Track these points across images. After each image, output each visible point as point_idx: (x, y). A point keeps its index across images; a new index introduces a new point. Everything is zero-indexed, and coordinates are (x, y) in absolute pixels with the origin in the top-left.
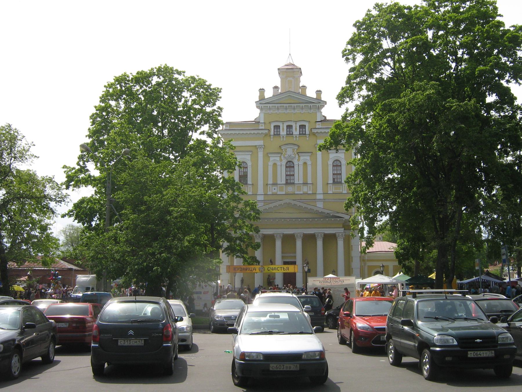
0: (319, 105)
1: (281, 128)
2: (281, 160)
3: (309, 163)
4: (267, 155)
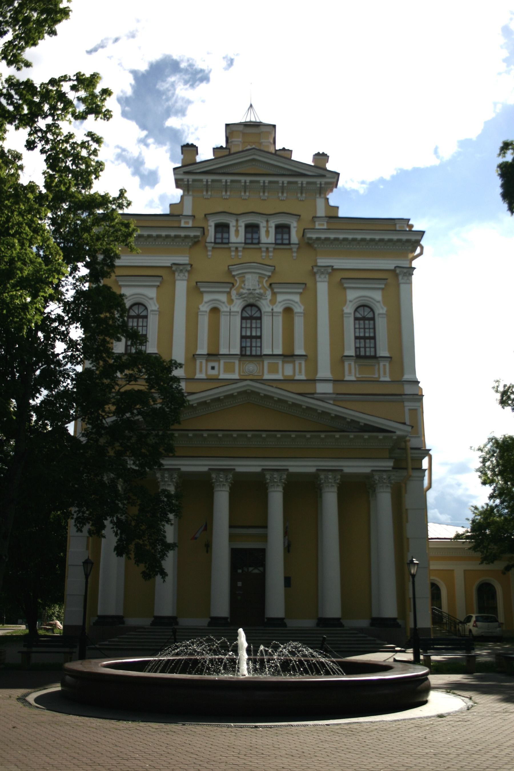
0: (323, 180)
1: (232, 230)
2: (231, 301)
3: (298, 309)
4: (196, 290)
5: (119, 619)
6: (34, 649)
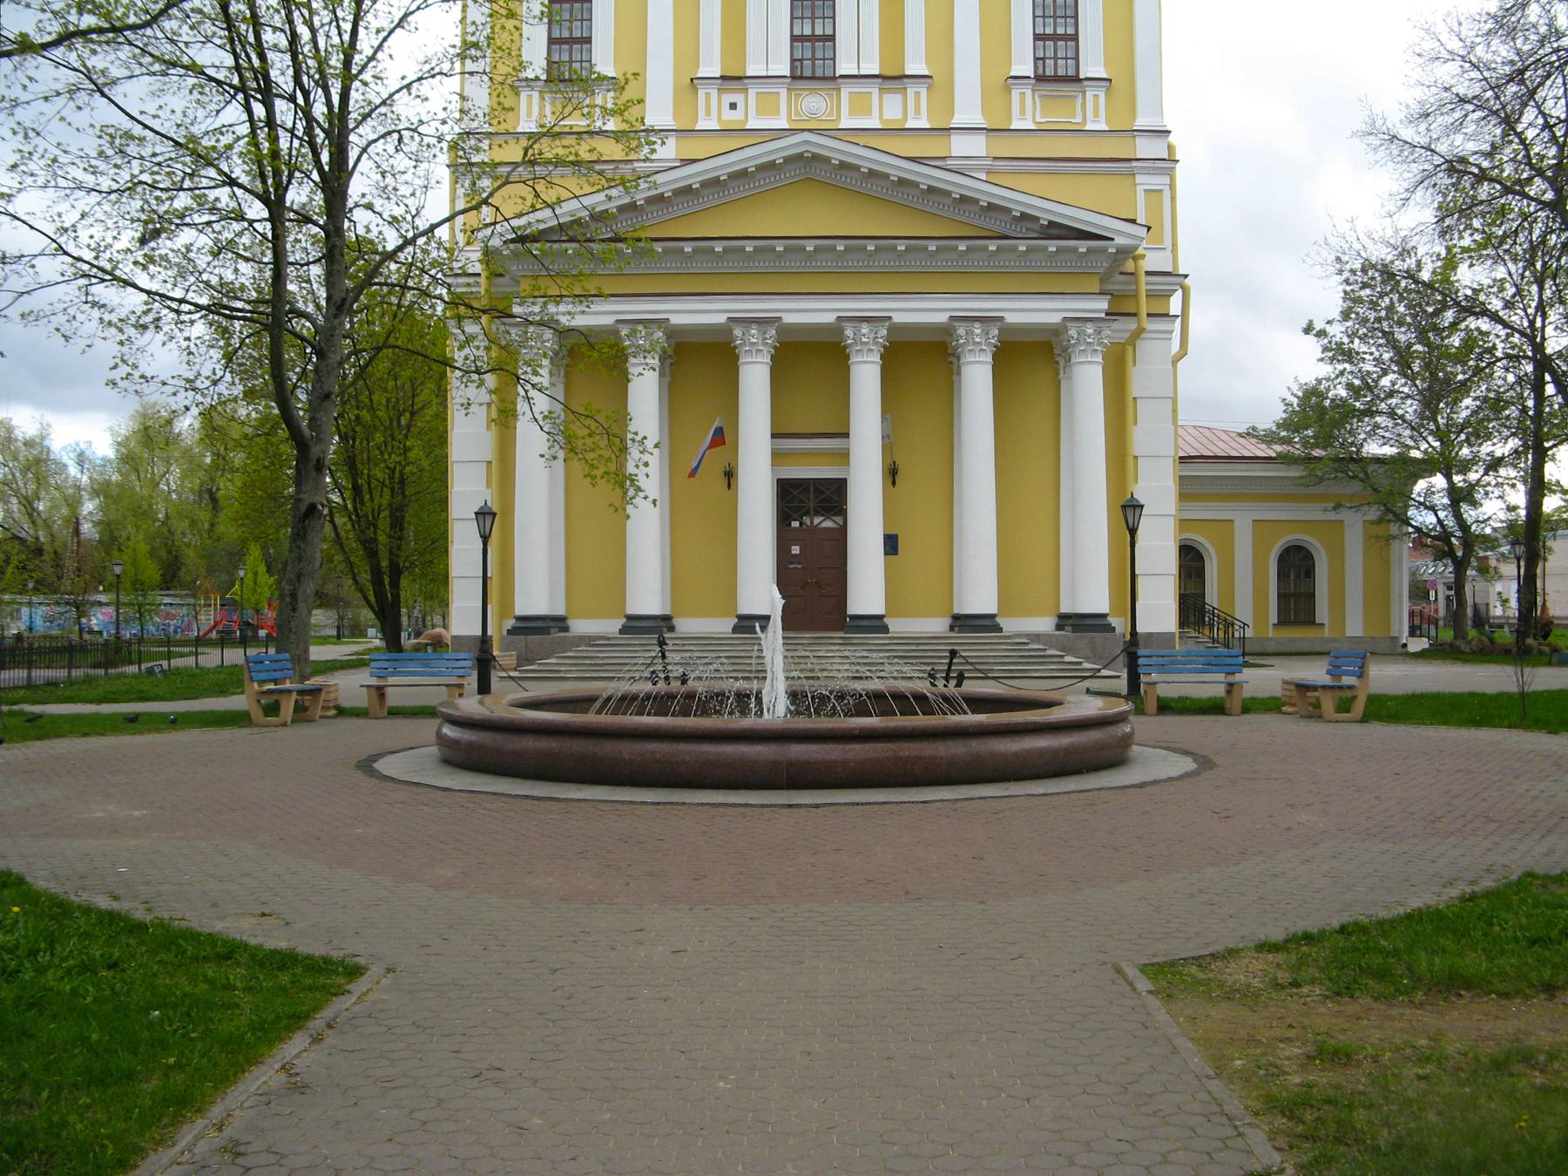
5: (560, 622)
6: (391, 680)
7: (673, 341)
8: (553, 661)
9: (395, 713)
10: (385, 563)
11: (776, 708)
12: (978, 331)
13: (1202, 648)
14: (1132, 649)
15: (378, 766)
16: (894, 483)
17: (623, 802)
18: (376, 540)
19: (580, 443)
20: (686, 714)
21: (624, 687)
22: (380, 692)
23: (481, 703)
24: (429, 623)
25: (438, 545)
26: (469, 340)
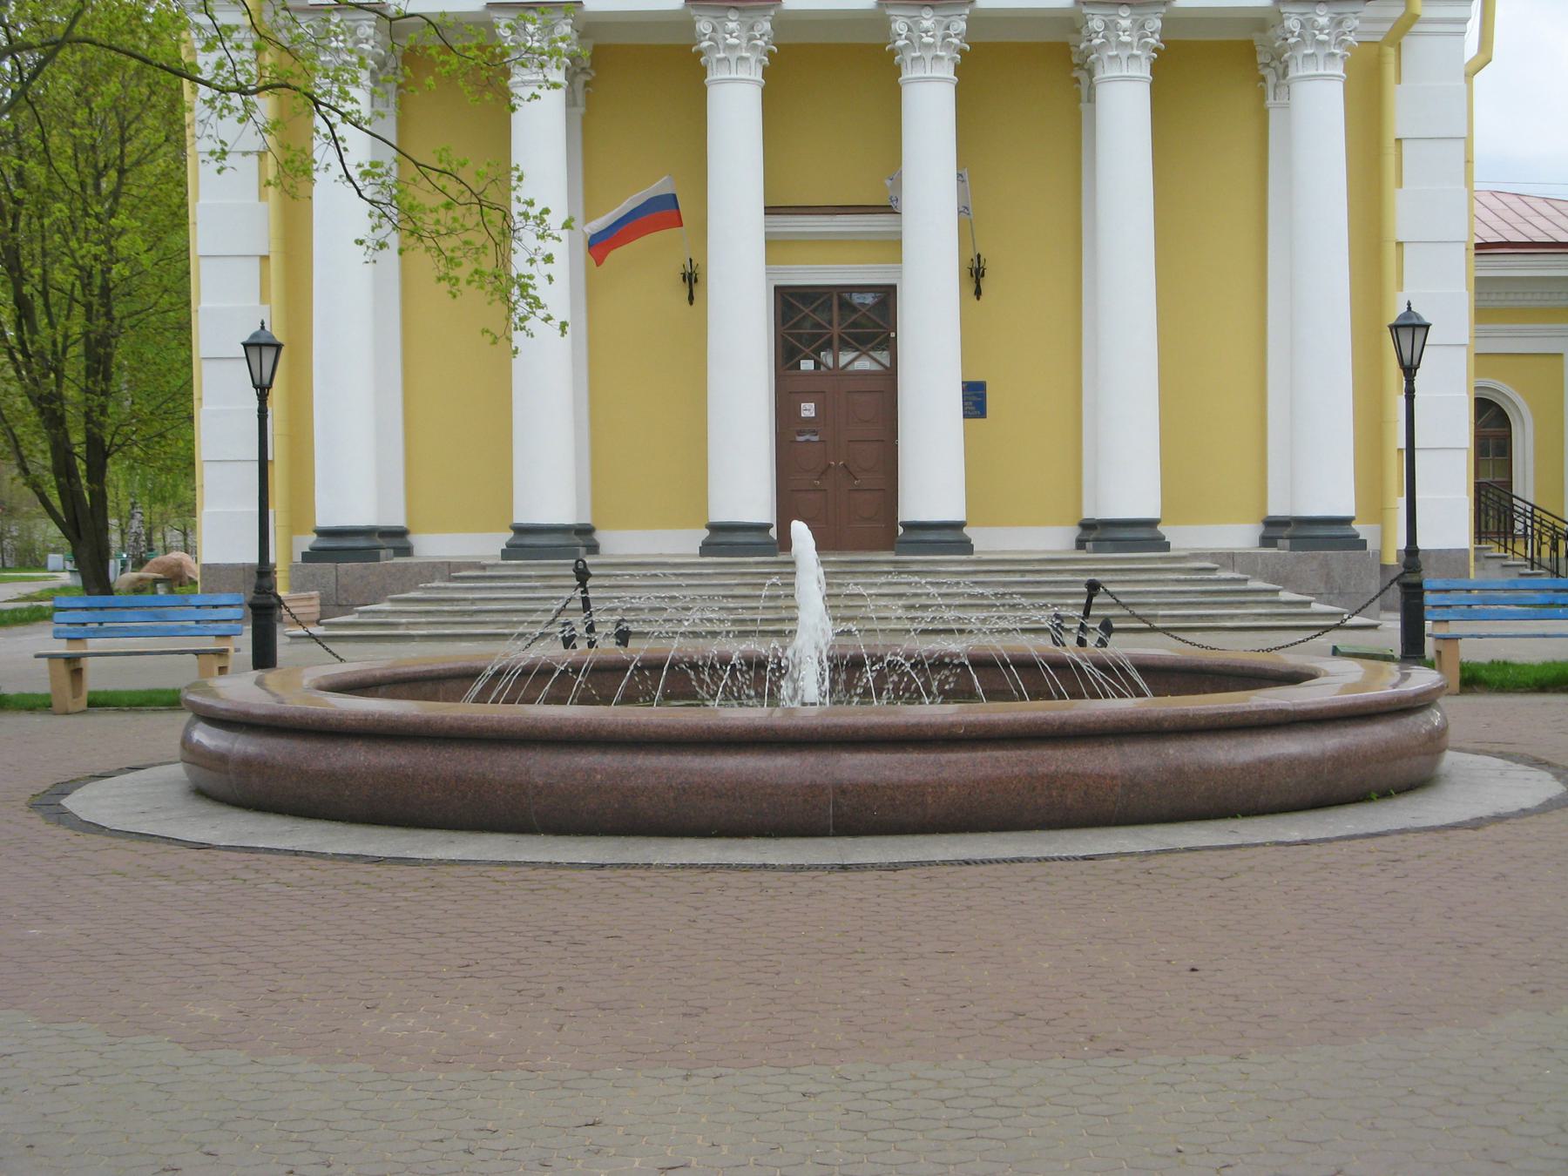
5: (397, 539)
6: (94, 644)
7: (590, 42)
8: (386, 606)
9: (99, 703)
10: (77, 438)
11: (807, 691)
12: (1125, 23)
13: (1512, 576)
14: (1413, 579)
15: (68, 802)
16: (978, 293)
17: (534, 865)
18: (59, 397)
19: (429, 219)
20: (561, 701)
21: (518, 654)
22: (73, 666)
23: (260, 683)
24: (158, 544)
25: (175, 406)
26: (223, 33)
